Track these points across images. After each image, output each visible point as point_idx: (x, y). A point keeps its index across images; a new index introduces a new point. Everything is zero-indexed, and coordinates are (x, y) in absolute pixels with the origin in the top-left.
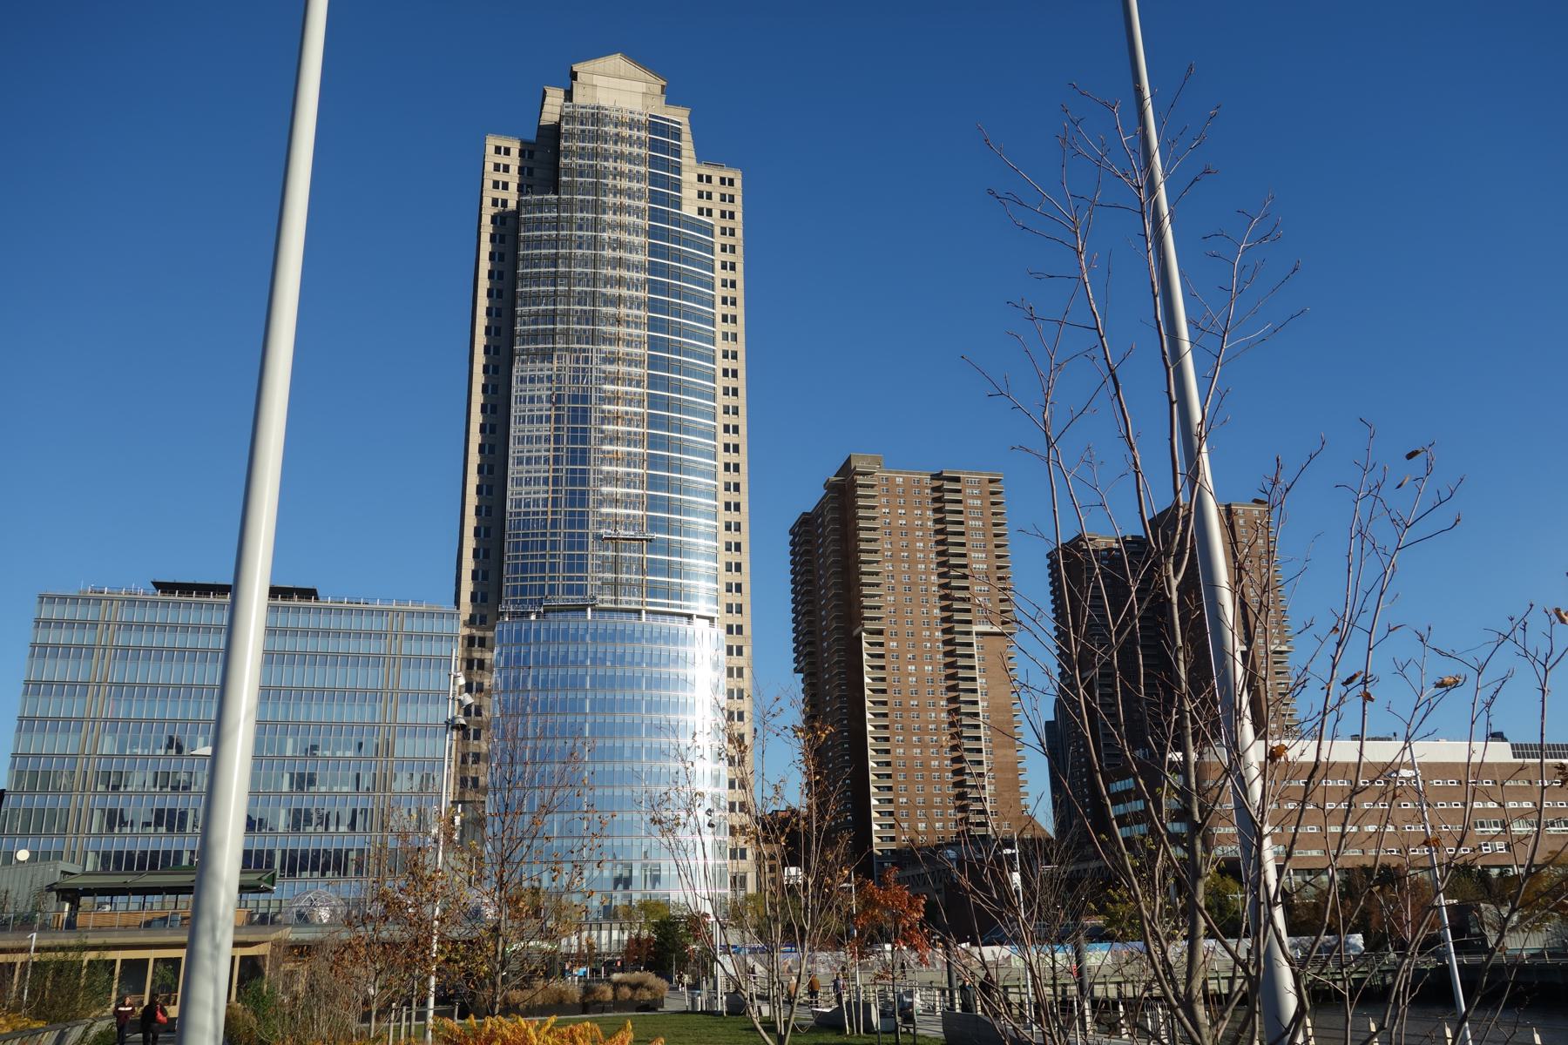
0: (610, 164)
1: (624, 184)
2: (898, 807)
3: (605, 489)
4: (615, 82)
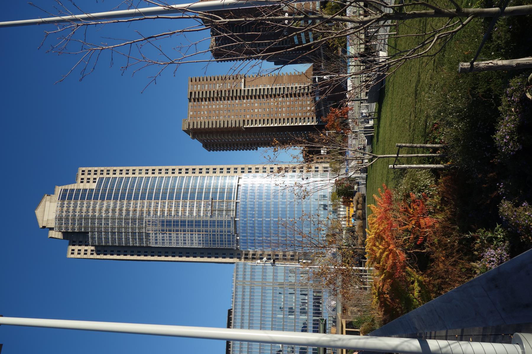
0: (77, 214)
1: (84, 209)
2: (302, 116)
3: (195, 214)
4: (46, 213)
